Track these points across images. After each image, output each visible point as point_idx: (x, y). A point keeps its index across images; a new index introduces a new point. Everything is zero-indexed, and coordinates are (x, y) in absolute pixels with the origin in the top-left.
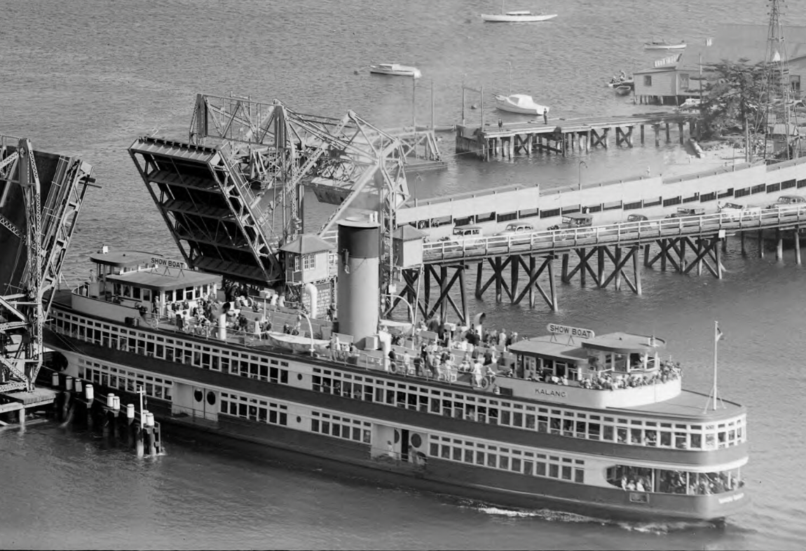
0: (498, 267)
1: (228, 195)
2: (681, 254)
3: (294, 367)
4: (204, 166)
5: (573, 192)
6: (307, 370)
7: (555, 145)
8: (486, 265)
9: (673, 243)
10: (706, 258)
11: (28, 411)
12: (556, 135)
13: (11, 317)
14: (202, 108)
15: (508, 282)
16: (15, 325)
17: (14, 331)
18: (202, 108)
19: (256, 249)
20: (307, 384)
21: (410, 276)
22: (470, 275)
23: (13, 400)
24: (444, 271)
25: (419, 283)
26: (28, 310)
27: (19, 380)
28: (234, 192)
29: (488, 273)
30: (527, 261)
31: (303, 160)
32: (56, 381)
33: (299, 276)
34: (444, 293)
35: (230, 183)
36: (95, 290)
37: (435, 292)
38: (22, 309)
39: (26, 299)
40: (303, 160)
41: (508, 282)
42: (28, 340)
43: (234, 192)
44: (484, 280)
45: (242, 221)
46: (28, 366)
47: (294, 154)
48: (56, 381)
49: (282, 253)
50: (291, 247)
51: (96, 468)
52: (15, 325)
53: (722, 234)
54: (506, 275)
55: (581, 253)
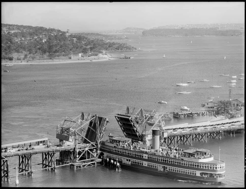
0: (181, 137)
1: (133, 124)
3: (144, 155)
6: (147, 155)
9: (212, 133)
10: (218, 135)
11: (97, 163)
13: (94, 146)
14: (128, 109)
15: (183, 140)
16: (94, 147)
17: (94, 149)
18: (128, 109)
19: (138, 134)
20: (147, 158)
23: (94, 161)
26: (97, 145)
27: (95, 157)
28: (134, 124)
30: (186, 136)
32: (102, 157)
35: (133, 122)
36: (109, 141)
37: (170, 142)
42: (97, 150)
43: (134, 124)
46: (97, 155)
48: (102, 157)
52: (94, 147)
54: (182, 138)
55: (195, 135)
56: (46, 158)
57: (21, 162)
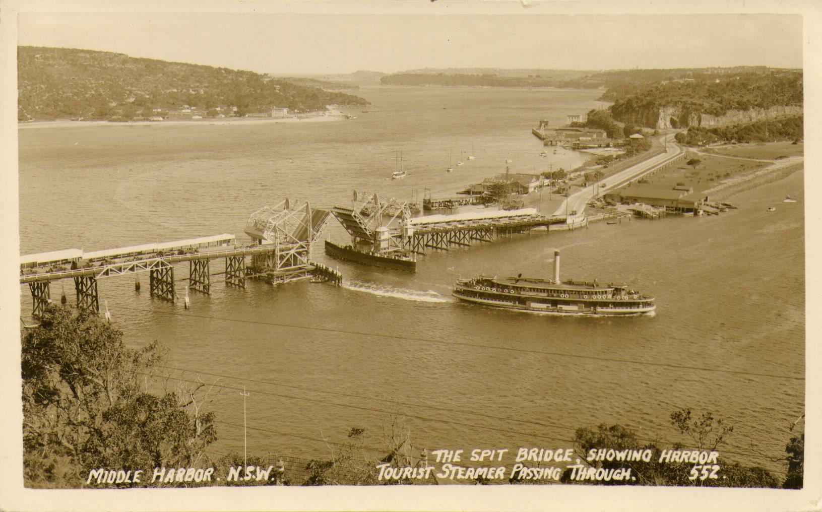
2: (481, 233)
4: (350, 216)
5: (21, 426)
7: (384, 242)
8: (430, 235)
12: (450, 201)
13: (303, 248)
19: (368, 233)
21: (410, 238)
22: (425, 237)
24: (419, 237)
25: (412, 240)
29: (430, 237)
30: (440, 234)
31: (382, 207)
33: (380, 238)
34: (419, 242)
38: (306, 245)
39: (308, 242)
40: (382, 207)
41: (436, 240)
44: (429, 239)
45: (363, 227)
47: (380, 206)
49: (376, 232)
50: (377, 230)
51: (80, 85)
53: (492, 228)
56: (231, 264)
57: (193, 270)
